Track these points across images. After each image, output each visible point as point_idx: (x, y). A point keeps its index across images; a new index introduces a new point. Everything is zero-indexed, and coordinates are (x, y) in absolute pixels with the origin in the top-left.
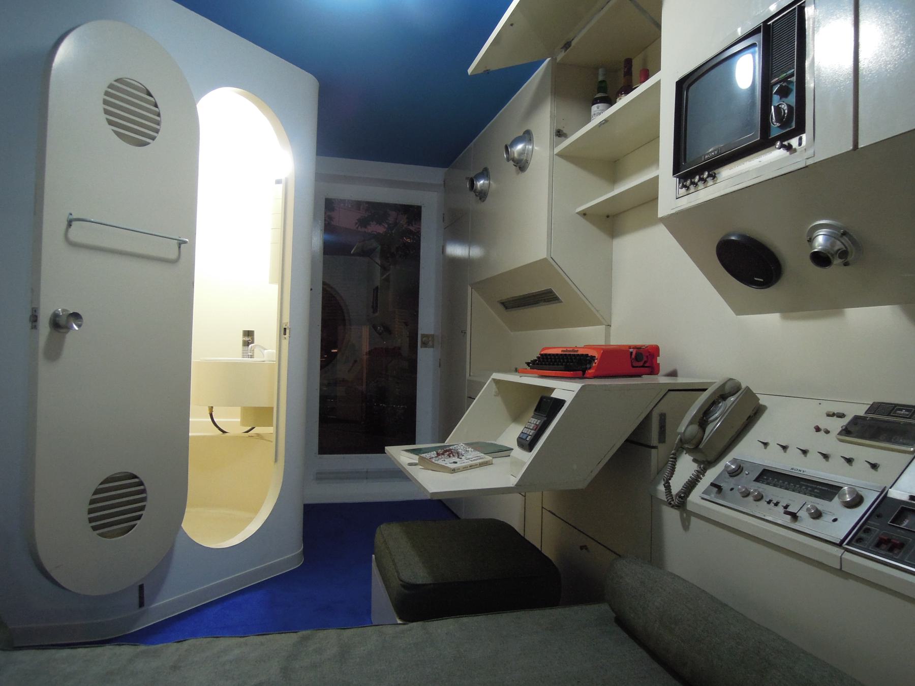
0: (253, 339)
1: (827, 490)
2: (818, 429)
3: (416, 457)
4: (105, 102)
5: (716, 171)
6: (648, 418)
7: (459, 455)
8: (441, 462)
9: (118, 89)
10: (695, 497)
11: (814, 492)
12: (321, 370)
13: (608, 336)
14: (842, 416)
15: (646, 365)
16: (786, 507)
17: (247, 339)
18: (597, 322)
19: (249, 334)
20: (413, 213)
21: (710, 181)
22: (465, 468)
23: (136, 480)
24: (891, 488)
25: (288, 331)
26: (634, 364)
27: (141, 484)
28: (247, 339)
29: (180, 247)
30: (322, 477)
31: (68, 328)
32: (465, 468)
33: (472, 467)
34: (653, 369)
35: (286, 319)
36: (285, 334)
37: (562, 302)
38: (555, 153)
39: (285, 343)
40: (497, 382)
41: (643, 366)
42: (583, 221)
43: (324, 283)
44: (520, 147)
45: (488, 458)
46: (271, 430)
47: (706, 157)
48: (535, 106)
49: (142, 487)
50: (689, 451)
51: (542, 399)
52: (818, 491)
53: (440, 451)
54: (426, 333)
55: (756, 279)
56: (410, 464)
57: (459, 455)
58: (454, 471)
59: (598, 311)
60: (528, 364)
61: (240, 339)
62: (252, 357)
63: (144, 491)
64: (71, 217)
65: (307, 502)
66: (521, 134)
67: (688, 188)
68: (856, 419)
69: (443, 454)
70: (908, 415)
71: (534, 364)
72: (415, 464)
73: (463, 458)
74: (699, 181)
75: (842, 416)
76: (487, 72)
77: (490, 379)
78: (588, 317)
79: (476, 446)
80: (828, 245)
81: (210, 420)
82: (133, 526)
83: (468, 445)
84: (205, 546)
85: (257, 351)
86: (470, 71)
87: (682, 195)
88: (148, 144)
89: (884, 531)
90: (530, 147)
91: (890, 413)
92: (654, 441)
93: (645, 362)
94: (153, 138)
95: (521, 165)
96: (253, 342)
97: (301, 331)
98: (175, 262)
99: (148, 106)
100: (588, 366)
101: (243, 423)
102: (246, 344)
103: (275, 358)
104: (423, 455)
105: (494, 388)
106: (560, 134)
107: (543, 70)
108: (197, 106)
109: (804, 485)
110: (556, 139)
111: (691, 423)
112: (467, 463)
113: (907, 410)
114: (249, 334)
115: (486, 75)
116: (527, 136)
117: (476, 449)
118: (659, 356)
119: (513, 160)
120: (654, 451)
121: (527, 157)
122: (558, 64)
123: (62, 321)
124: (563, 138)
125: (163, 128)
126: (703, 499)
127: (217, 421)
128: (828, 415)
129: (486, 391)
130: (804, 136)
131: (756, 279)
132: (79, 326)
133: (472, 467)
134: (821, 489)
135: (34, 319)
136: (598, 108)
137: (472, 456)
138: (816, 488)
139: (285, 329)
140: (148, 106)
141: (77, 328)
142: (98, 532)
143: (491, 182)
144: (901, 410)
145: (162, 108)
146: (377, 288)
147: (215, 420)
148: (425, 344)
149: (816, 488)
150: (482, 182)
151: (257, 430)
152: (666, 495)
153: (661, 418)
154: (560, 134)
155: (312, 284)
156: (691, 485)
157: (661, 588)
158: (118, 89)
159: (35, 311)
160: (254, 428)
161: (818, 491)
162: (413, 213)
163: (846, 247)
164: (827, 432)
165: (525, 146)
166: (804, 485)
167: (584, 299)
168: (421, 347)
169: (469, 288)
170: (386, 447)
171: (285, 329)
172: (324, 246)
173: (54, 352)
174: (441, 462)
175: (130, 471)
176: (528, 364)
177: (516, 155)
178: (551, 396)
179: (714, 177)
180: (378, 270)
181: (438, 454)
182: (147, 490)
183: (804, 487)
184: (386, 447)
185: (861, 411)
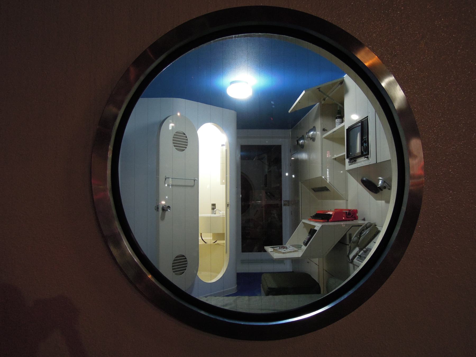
0: (215, 207)
3: (273, 249)
4: (174, 143)
5: (356, 159)
6: (346, 235)
7: (287, 248)
8: (280, 250)
9: (177, 135)
12: (242, 214)
13: (347, 204)
15: (352, 217)
17: (213, 207)
18: (343, 199)
19: (214, 205)
20: (278, 149)
22: (288, 252)
23: (184, 257)
25: (229, 205)
26: (348, 217)
27: (186, 258)
28: (213, 207)
29: (194, 181)
30: (243, 262)
31: (167, 210)
32: (288, 252)
33: (290, 252)
34: (356, 218)
35: (228, 201)
36: (228, 206)
37: (330, 191)
38: (323, 137)
39: (228, 210)
40: (304, 223)
42: (334, 161)
43: (242, 173)
44: (312, 133)
45: (296, 249)
46: (224, 242)
48: (316, 119)
49: (186, 260)
51: (311, 229)
53: (281, 247)
54: (285, 200)
56: (271, 252)
57: (287, 248)
58: (284, 253)
59: (342, 195)
60: (311, 217)
61: (210, 207)
62: (215, 214)
63: (186, 261)
64: (166, 177)
65: (237, 272)
66: (312, 128)
69: (281, 248)
71: (313, 217)
72: (273, 252)
73: (288, 249)
76: (296, 111)
77: (301, 222)
78: (338, 197)
79: (293, 246)
80: (382, 185)
81: (201, 238)
82: (184, 272)
83: (291, 245)
84: (204, 281)
85: (217, 212)
86: (289, 111)
88: (185, 150)
90: (315, 133)
93: (352, 216)
94: (186, 148)
95: (313, 139)
96: (215, 208)
97: (234, 204)
98: (193, 186)
99: (181, 135)
100: (330, 218)
101: (213, 239)
102: (213, 209)
103: (225, 214)
104: (275, 248)
105: (303, 225)
106: (324, 130)
107: (317, 107)
108: (197, 132)
111: (355, 236)
112: (288, 250)
114: (214, 205)
115: (294, 112)
116: (314, 129)
117: (293, 247)
119: (309, 137)
121: (314, 136)
122: (323, 104)
123: (165, 209)
124: (326, 131)
125: (189, 144)
126: (357, 260)
127: (204, 239)
129: (301, 225)
132: (170, 210)
133: (290, 252)
135: (158, 208)
136: (337, 120)
137: (292, 249)
139: (228, 205)
140: (181, 135)
141: (169, 210)
142: (175, 273)
143: (305, 141)
145: (187, 135)
146: (266, 175)
147: (203, 238)
148: (285, 205)
150: (302, 141)
151: (218, 242)
154: (324, 130)
155: (237, 186)
158: (177, 135)
159: (158, 206)
160: (216, 241)
162: (278, 149)
165: (313, 132)
167: (337, 191)
168: (284, 206)
169: (300, 183)
170: (265, 247)
171: (228, 205)
172: (241, 157)
173: (163, 218)
174: (280, 250)
175: (183, 255)
176: (311, 217)
177: (310, 136)
178: (315, 229)
179: (356, 161)
180: (267, 167)
181: (280, 248)
182: (188, 261)
184: (265, 247)
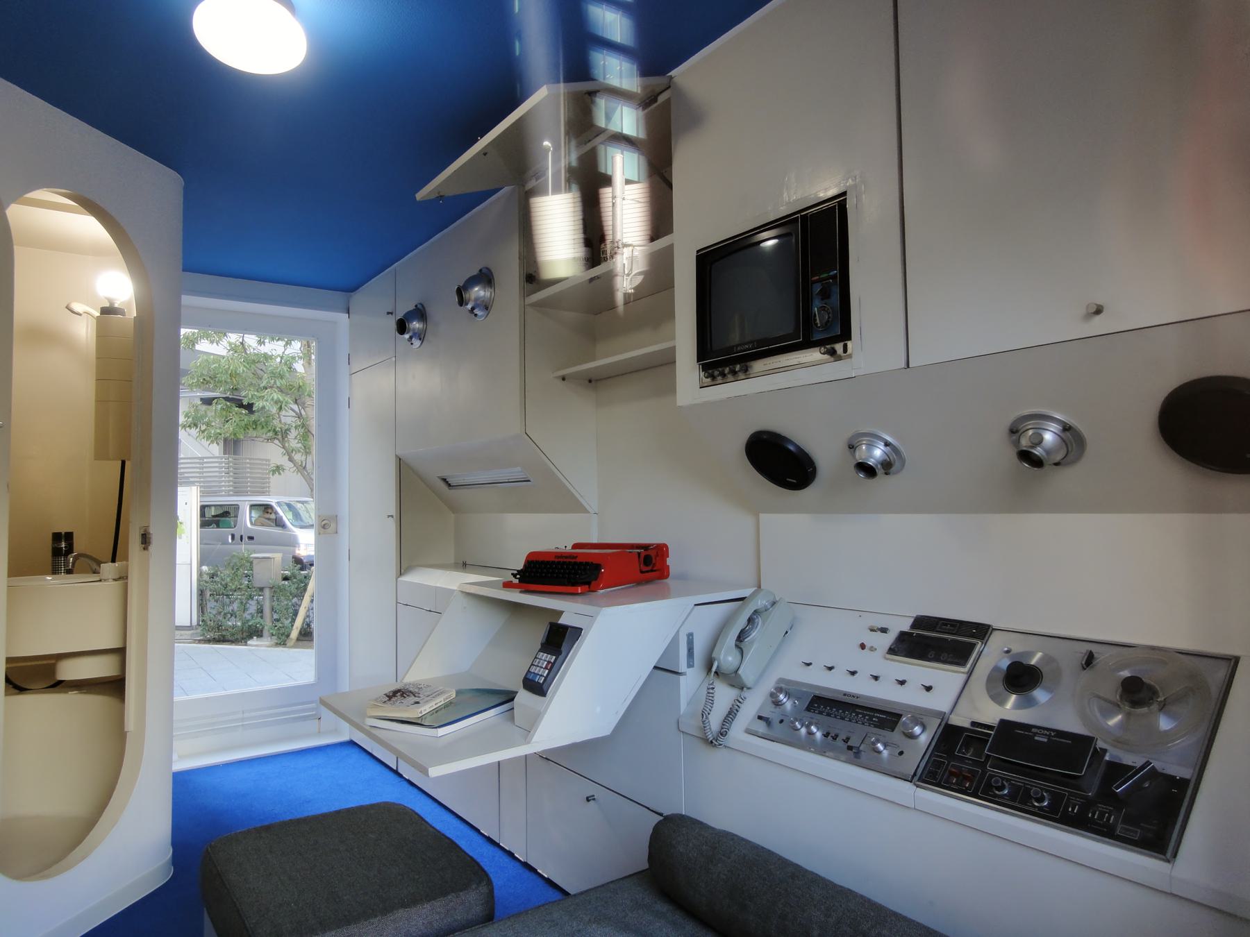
1: (886, 718)
2: (863, 646)
5: (748, 364)
10: (737, 732)
11: (873, 721)
14: (884, 630)
16: (846, 740)
19: (588, 800)
21: (742, 376)
24: (951, 714)
41: (652, 571)
47: (739, 348)
50: (193, 345)
52: (877, 720)
55: (795, 481)
67: (713, 377)
68: (902, 636)
70: (953, 630)
74: (729, 373)
75: (884, 630)
87: (706, 385)
89: (1001, 793)
91: (935, 627)
92: (683, 666)
109: (860, 713)
110: (529, 286)
113: (952, 625)
118: (668, 557)
120: (682, 678)
128: (872, 630)
130: (849, 344)
131: (795, 481)
134: (879, 717)
138: (874, 717)
144: (946, 625)
149: (874, 717)
152: (269, 487)
153: (688, 638)
156: (732, 714)
157: (724, 855)
161: (877, 720)
163: (889, 457)
164: (872, 649)
166: (860, 713)
178: (559, 622)
179: (746, 370)
183: (861, 716)
185: (906, 626)
